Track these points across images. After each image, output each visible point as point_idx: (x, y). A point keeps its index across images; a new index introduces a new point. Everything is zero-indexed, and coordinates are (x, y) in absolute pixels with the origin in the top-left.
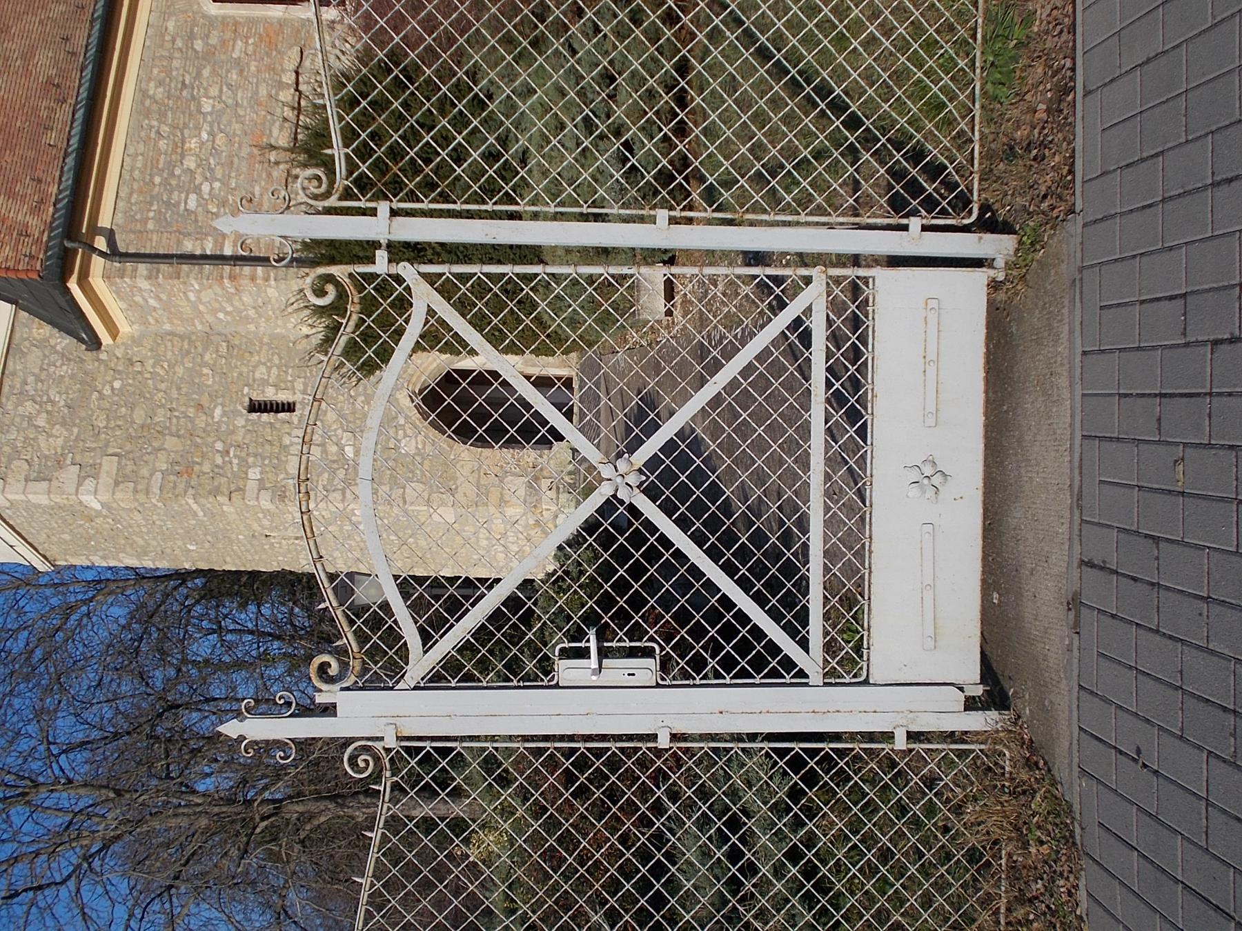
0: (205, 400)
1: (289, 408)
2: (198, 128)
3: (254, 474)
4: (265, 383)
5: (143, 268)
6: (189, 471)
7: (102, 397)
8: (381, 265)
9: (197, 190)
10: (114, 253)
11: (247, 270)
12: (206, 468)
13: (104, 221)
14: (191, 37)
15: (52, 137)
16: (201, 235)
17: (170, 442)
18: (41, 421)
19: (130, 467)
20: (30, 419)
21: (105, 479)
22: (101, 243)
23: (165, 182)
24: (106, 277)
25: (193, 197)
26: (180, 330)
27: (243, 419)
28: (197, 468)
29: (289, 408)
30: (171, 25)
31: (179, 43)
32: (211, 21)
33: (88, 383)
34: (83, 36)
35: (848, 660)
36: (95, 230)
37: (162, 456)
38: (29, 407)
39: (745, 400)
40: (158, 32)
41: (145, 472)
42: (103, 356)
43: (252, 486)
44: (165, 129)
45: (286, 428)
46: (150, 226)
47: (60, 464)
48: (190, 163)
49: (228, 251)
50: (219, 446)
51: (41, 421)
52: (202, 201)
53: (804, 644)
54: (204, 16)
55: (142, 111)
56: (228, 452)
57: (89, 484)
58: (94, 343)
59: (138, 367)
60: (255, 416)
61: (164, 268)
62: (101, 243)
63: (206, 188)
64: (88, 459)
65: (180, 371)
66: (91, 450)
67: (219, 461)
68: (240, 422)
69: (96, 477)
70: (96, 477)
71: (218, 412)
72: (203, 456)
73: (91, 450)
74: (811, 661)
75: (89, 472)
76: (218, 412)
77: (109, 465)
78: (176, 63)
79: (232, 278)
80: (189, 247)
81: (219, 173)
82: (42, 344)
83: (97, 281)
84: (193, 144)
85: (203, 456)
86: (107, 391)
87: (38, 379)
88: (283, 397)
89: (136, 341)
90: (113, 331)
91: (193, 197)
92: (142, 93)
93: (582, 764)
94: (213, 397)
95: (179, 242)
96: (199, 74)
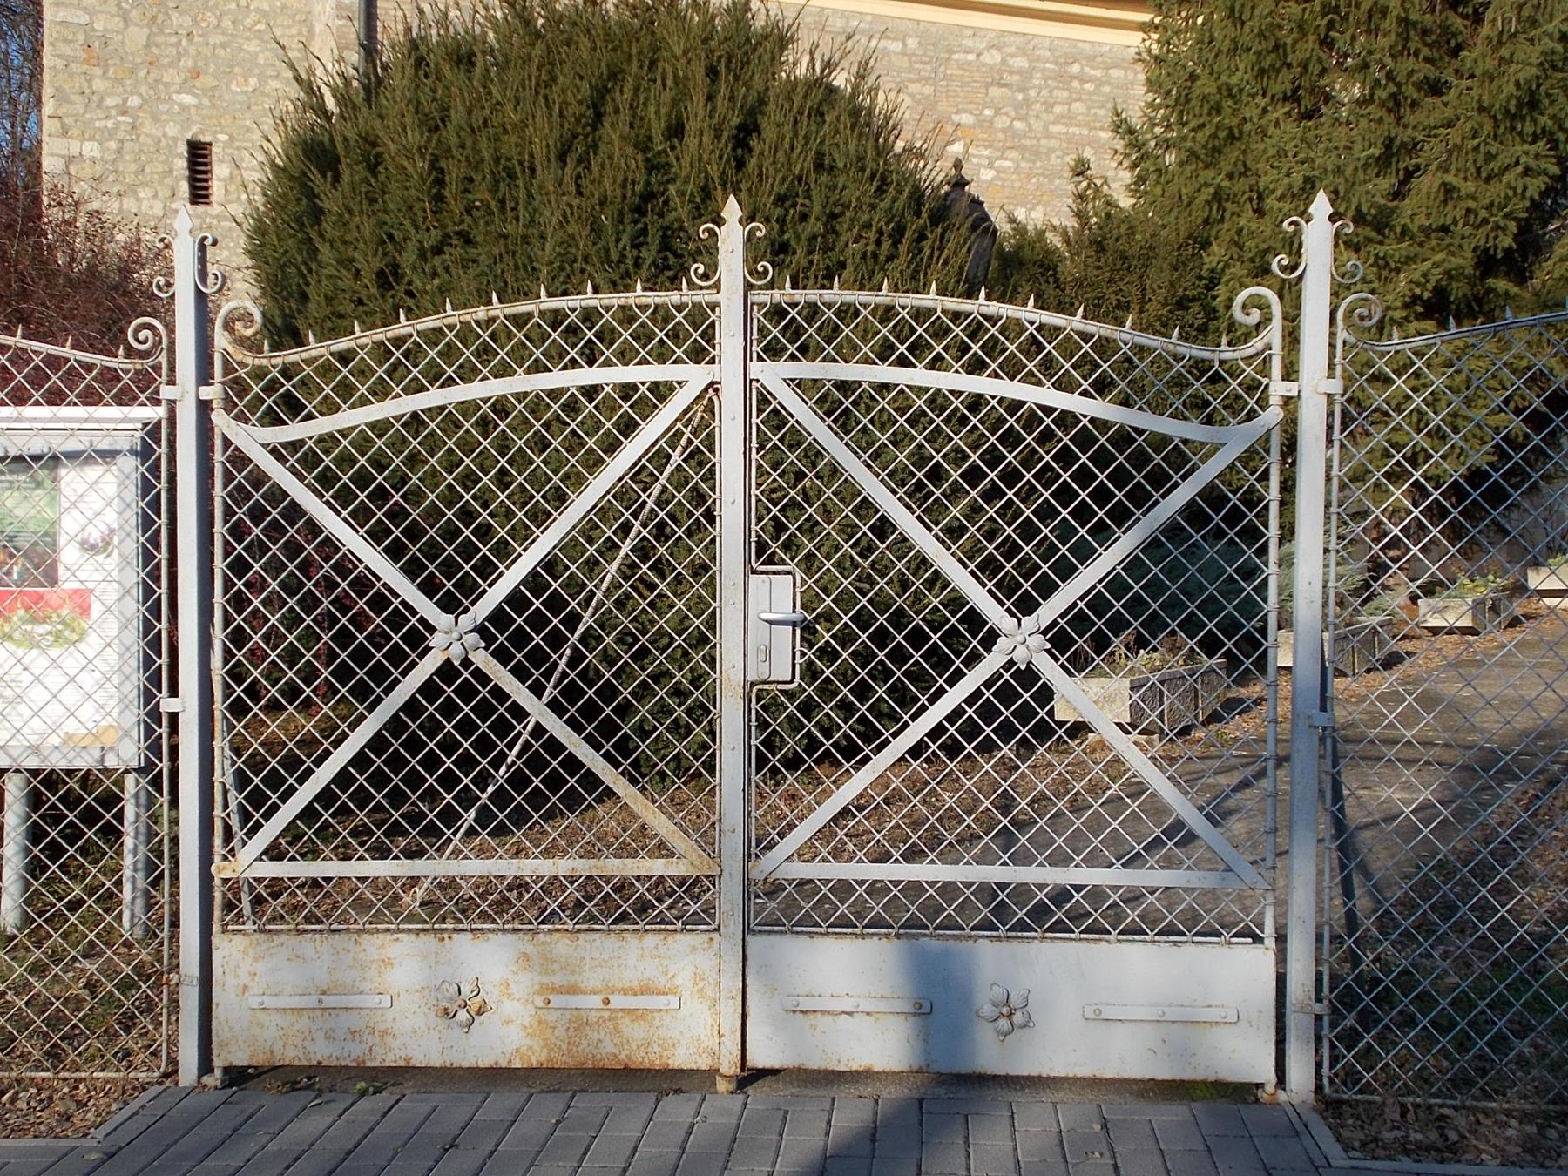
0: (206, 81)
1: (199, 194)
3: (90, 149)
6: (98, 61)
8: (1278, 388)
12: (99, 84)
17: (137, 35)
28: (98, 71)
29: (199, 194)
35: (226, 904)
45: (164, 192)
50: (134, 101)
56: (124, 113)
60: (183, 149)
67: (110, 101)
68: (172, 130)
71: (188, 99)
72: (118, 81)
74: (248, 862)
76: (188, 99)
88: (217, 189)
94: (211, 92)
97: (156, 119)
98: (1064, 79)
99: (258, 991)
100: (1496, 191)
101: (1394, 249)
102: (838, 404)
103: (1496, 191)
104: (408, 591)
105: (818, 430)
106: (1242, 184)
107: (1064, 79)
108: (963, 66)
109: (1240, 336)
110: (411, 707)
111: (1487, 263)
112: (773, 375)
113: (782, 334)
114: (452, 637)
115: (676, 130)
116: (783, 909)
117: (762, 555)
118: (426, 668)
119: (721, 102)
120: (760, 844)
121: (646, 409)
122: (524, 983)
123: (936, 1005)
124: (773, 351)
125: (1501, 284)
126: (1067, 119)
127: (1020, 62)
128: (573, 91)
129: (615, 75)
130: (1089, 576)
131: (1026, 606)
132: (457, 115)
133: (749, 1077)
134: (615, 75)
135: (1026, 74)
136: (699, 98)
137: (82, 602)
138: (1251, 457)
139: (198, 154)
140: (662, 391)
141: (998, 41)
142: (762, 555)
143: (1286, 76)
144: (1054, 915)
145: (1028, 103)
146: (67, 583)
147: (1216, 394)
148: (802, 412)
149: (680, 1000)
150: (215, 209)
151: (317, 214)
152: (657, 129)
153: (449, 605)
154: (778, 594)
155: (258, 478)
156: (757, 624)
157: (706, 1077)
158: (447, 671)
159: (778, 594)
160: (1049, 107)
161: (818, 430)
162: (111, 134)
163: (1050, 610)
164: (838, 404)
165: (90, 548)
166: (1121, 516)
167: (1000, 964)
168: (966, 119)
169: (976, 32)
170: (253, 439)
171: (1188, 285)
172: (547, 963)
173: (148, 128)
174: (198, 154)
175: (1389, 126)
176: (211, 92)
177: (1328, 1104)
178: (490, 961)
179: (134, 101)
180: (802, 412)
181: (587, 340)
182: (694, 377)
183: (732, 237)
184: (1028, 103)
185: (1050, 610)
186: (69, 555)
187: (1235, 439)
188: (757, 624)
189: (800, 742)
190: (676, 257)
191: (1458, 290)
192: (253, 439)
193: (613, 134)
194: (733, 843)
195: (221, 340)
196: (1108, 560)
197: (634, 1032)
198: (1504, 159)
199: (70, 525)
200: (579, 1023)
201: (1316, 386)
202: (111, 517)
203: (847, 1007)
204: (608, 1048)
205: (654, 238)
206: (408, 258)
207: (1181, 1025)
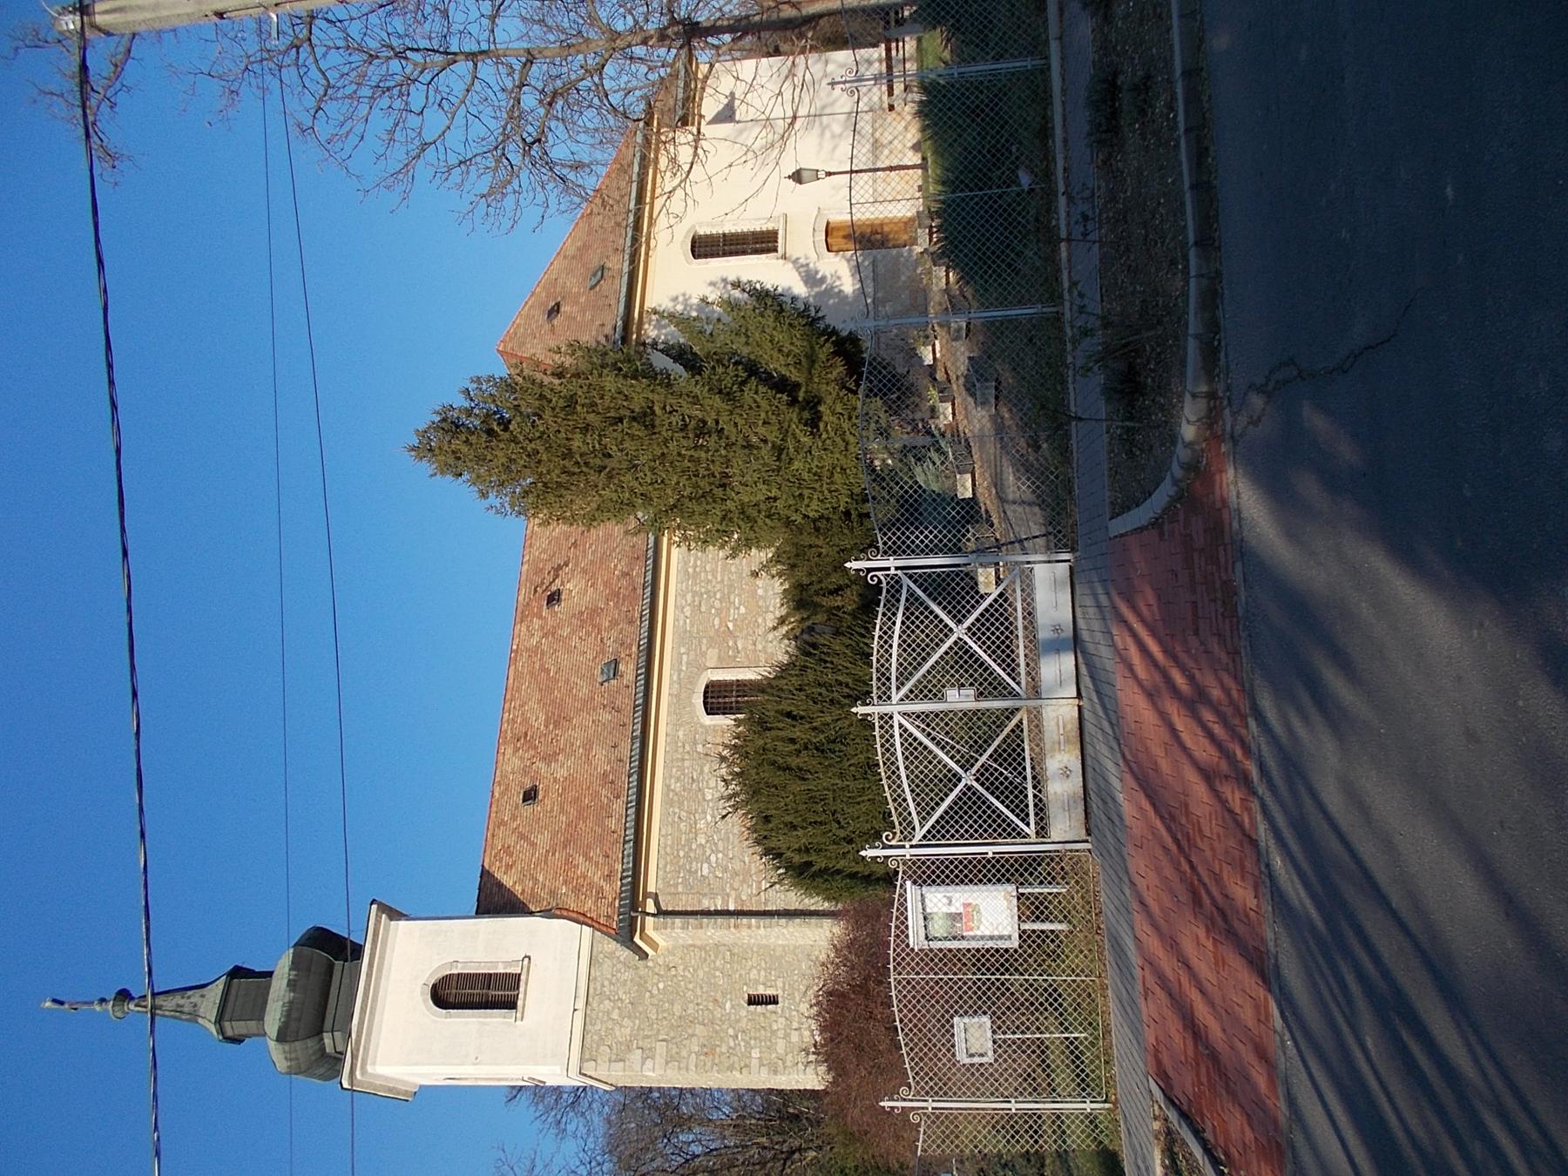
1: (773, 1000)
2: (704, 812)
3: (755, 1054)
4: (757, 982)
5: (678, 921)
6: (713, 1048)
7: (652, 996)
8: (893, 571)
9: (708, 860)
10: (661, 913)
11: (745, 921)
12: (724, 1049)
13: (651, 888)
14: (695, 743)
15: (612, 824)
16: (713, 896)
17: (699, 1029)
18: (615, 1015)
19: (675, 1050)
20: (608, 1013)
21: (660, 1060)
22: (650, 907)
23: (687, 856)
24: (655, 929)
25: (705, 866)
26: (698, 943)
27: (747, 1011)
29: (773, 1000)
30: (681, 733)
31: (687, 748)
32: (706, 729)
33: (641, 984)
34: (626, 749)
35: (1042, 831)
36: (646, 895)
37: (694, 1039)
38: (607, 1005)
39: (972, 656)
40: (673, 739)
41: (684, 1053)
42: (650, 964)
43: (755, 1063)
44: (683, 814)
45: (774, 1017)
46: (680, 889)
47: (629, 1049)
48: (702, 840)
49: (732, 908)
50: (731, 1032)
51: (615, 1015)
52: (712, 870)
53: (1028, 825)
54: (702, 726)
55: (668, 802)
57: (649, 1063)
58: (644, 956)
59: (673, 972)
60: (752, 1007)
61: (692, 920)
62: (650, 907)
63: (713, 858)
64: (646, 1044)
65: (701, 973)
66: (648, 1037)
68: (743, 1013)
69: (653, 1058)
70: (653, 1058)
71: (728, 1005)
72: (722, 1040)
73: (648, 1037)
74: (1031, 831)
75: (648, 1054)
76: (728, 1005)
77: (661, 1048)
78: (687, 764)
79: (736, 926)
80: (706, 904)
81: (721, 846)
82: (611, 956)
83: (649, 931)
84: (701, 824)
85: (722, 1040)
86: (655, 992)
87: (611, 983)
88: (770, 992)
89: (671, 952)
90: (654, 946)
91: (705, 866)
92: (667, 787)
93: (946, 1094)
94: (724, 995)
95: (700, 902)
96: (702, 772)
97: (738, 1021)
98: (696, 575)
99: (1065, 828)
100: (764, 404)
101: (791, 444)
102: (903, 679)
103: (764, 404)
104: (957, 791)
105: (909, 685)
106: (763, 506)
107: (696, 575)
108: (692, 625)
109: (880, 581)
110: (987, 789)
111: (793, 402)
112: (895, 698)
113: (885, 697)
114: (968, 779)
115: (793, 741)
116: (1036, 691)
117: (942, 699)
118: (975, 784)
119: (781, 725)
120: (1017, 696)
121: (906, 730)
122: (1058, 757)
123: (1056, 647)
124: (889, 698)
125: (801, 395)
126: (714, 572)
127: (689, 597)
128: (779, 778)
129: (773, 763)
130: (943, 615)
131: (951, 630)
132: (788, 819)
133: (1079, 696)
134: (773, 763)
135: (695, 594)
136: (781, 733)
137: (966, 905)
138: (910, 577)
139: (754, 1001)
140: (901, 726)
141: (680, 608)
142: (942, 699)
143: (716, 491)
144: (1030, 614)
145: (708, 592)
146: (961, 910)
147: (895, 585)
148: (904, 690)
149: (1060, 712)
150: (780, 993)
151: (827, 869)
152: (792, 747)
153: (960, 780)
154: (952, 694)
155: (929, 832)
156: (959, 699)
157: (1080, 707)
158: (977, 780)
159: (952, 694)
160: (709, 581)
161: (909, 685)
162: (747, 1043)
163: (951, 624)
164: (903, 679)
165: (950, 903)
166: (927, 608)
167: (1043, 634)
168: (717, 622)
169: (676, 620)
170: (919, 834)
171: (809, 528)
172: (1053, 750)
173: (743, 1024)
174: (754, 1001)
175: (737, 448)
176: (724, 995)
177: (1073, 550)
178: (1053, 764)
179: (731, 1032)
180: (904, 690)
181: (889, 749)
182: (897, 718)
183: (860, 710)
184: (708, 592)
185: (951, 624)
186: (953, 910)
187: (906, 581)
188: (959, 699)
189: (990, 687)
190: (866, 723)
191: (806, 415)
192: (919, 834)
193: (794, 762)
194: (1017, 703)
195: (893, 843)
196: (938, 610)
197: (1069, 727)
198: (750, 401)
199: (945, 910)
200: (1067, 741)
201: (891, 562)
202: (940, 896)
203: (1058, 669)
204: (1075, 733)
205: (831, 746)
206: (842, 833)
207: (1056, 583)
